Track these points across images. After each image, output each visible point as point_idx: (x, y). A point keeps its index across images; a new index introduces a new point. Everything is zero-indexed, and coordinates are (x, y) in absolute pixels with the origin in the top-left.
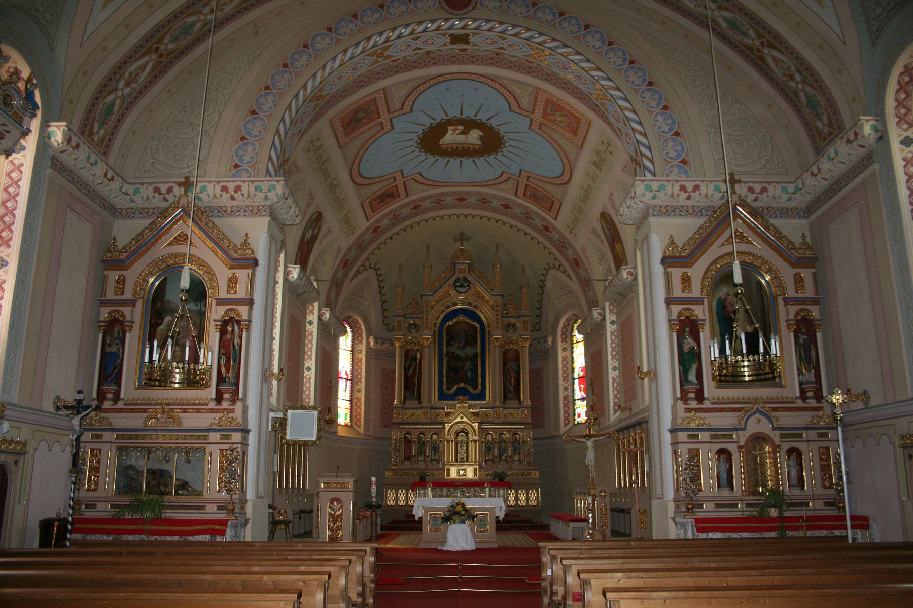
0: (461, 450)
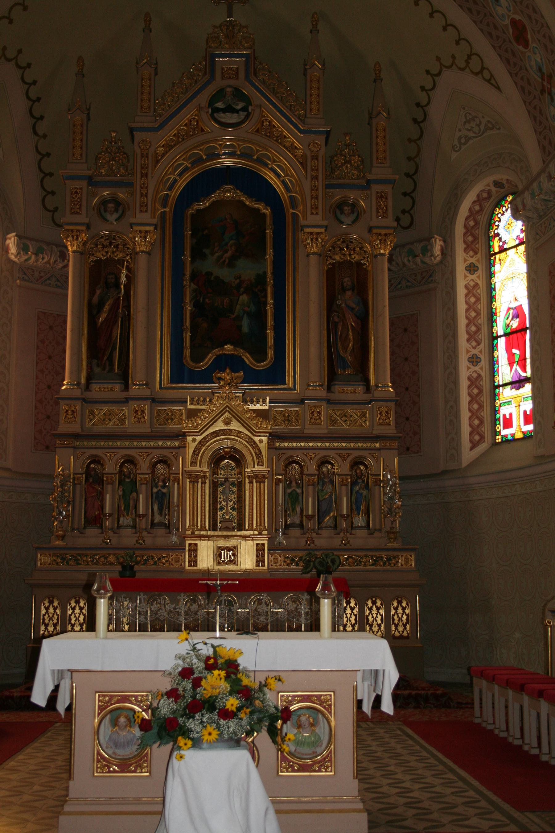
0: (226, 501)
